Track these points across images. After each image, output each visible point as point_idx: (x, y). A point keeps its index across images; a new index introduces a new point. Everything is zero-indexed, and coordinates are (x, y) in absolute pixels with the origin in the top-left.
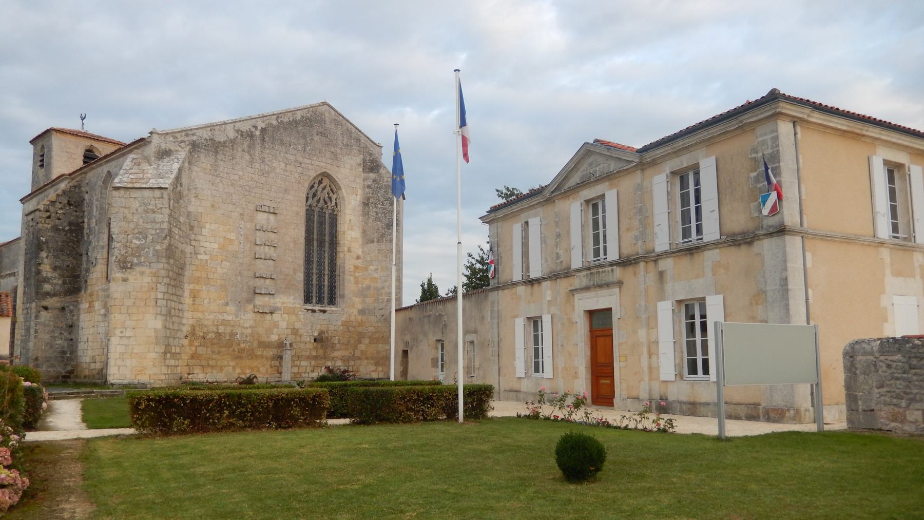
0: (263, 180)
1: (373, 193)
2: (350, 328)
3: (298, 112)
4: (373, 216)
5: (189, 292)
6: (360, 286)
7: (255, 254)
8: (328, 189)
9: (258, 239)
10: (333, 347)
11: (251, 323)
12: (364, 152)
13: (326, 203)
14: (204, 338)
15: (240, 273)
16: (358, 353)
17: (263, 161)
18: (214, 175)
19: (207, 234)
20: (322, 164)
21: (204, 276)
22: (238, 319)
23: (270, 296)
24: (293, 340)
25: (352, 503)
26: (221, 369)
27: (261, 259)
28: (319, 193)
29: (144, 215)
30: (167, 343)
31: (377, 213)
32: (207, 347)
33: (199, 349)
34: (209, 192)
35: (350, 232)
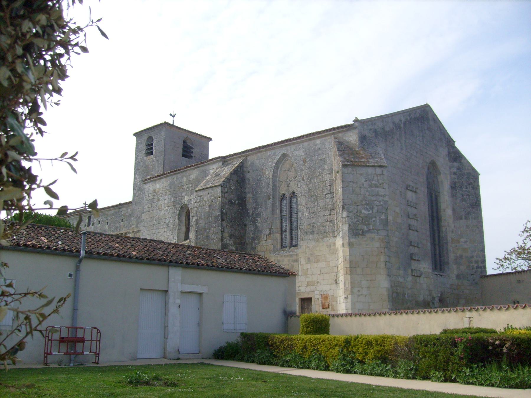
4: (460, 197)
29: (369, 189)
31: (463, 195)
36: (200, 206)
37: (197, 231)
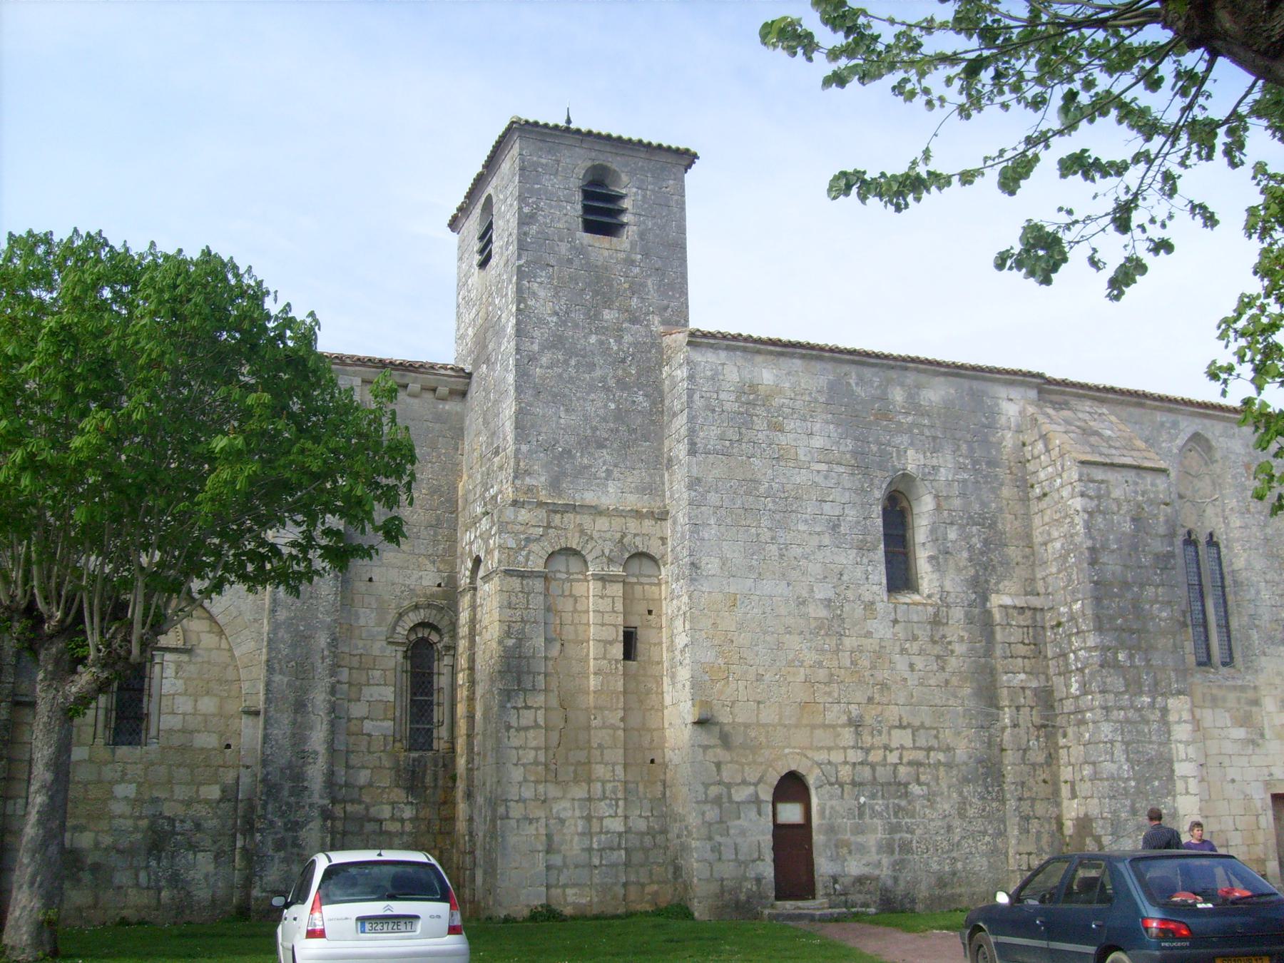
36: (1100, 512)
37: (1096, 583)
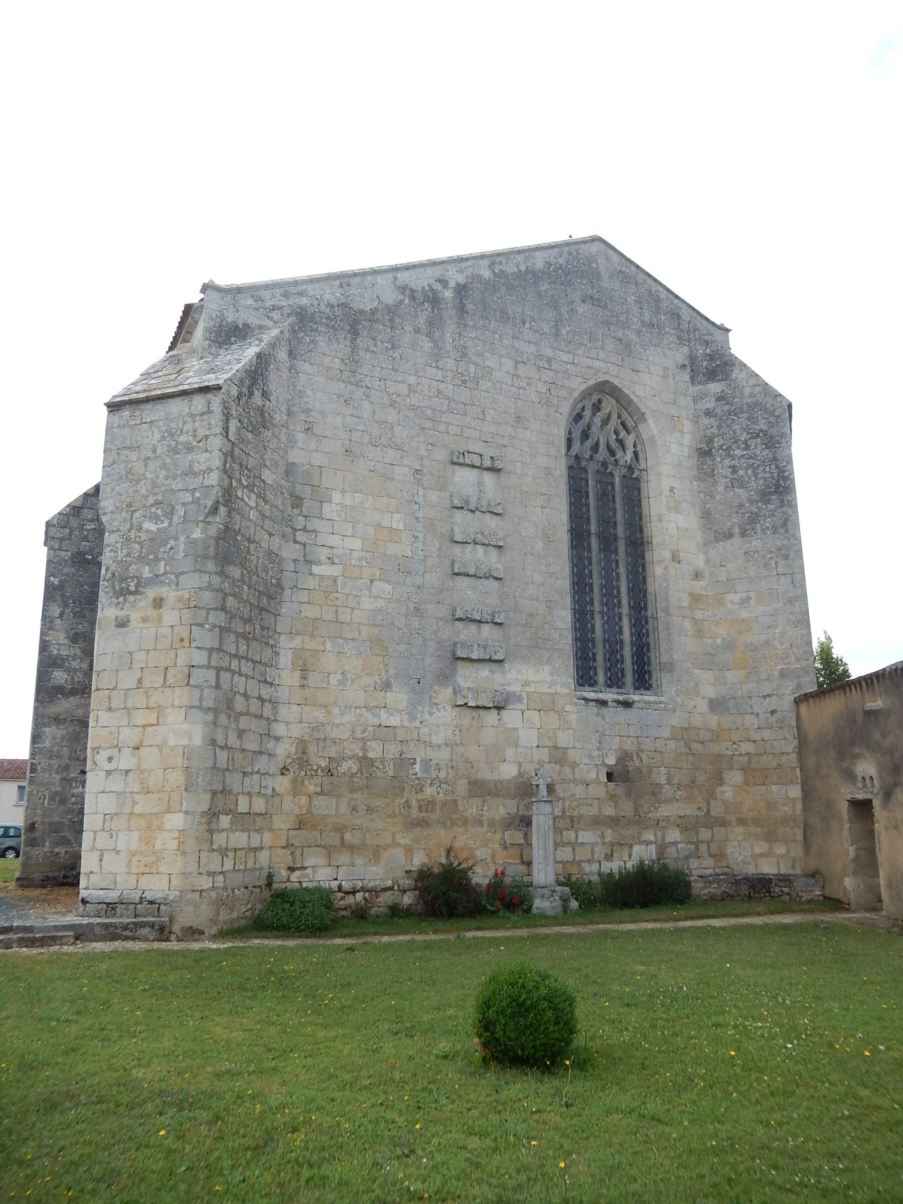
0: (464, 395)
1: (719, 427)
2: (694, 746)
3: (538, 254)
5: (290, 656)
6: (709, 641)
7: (453, 562)
8: (614, 421)
9: (456, 529)
10: (655, 792)
11: (450, 732)
12: (689, 341)
13: (612, 453)
14: (329, 772)
15: (417, 609)
16: (717, 810)
17: (463, 354)
18: (350, 383)
19: (334, 516)
20: (597, 364)
21: (330, 616)
22: (417, 724)
23: (494, 666)
24: (556, 777)
25: (335, 317)
26: (376, 854)
27: (468, 575)
28: (594, 429)
30: (218, 787)
31: (734, 469)
32: (338, 797)
33: (319, 801)
34: (339, 419)
35: (673, 516)
